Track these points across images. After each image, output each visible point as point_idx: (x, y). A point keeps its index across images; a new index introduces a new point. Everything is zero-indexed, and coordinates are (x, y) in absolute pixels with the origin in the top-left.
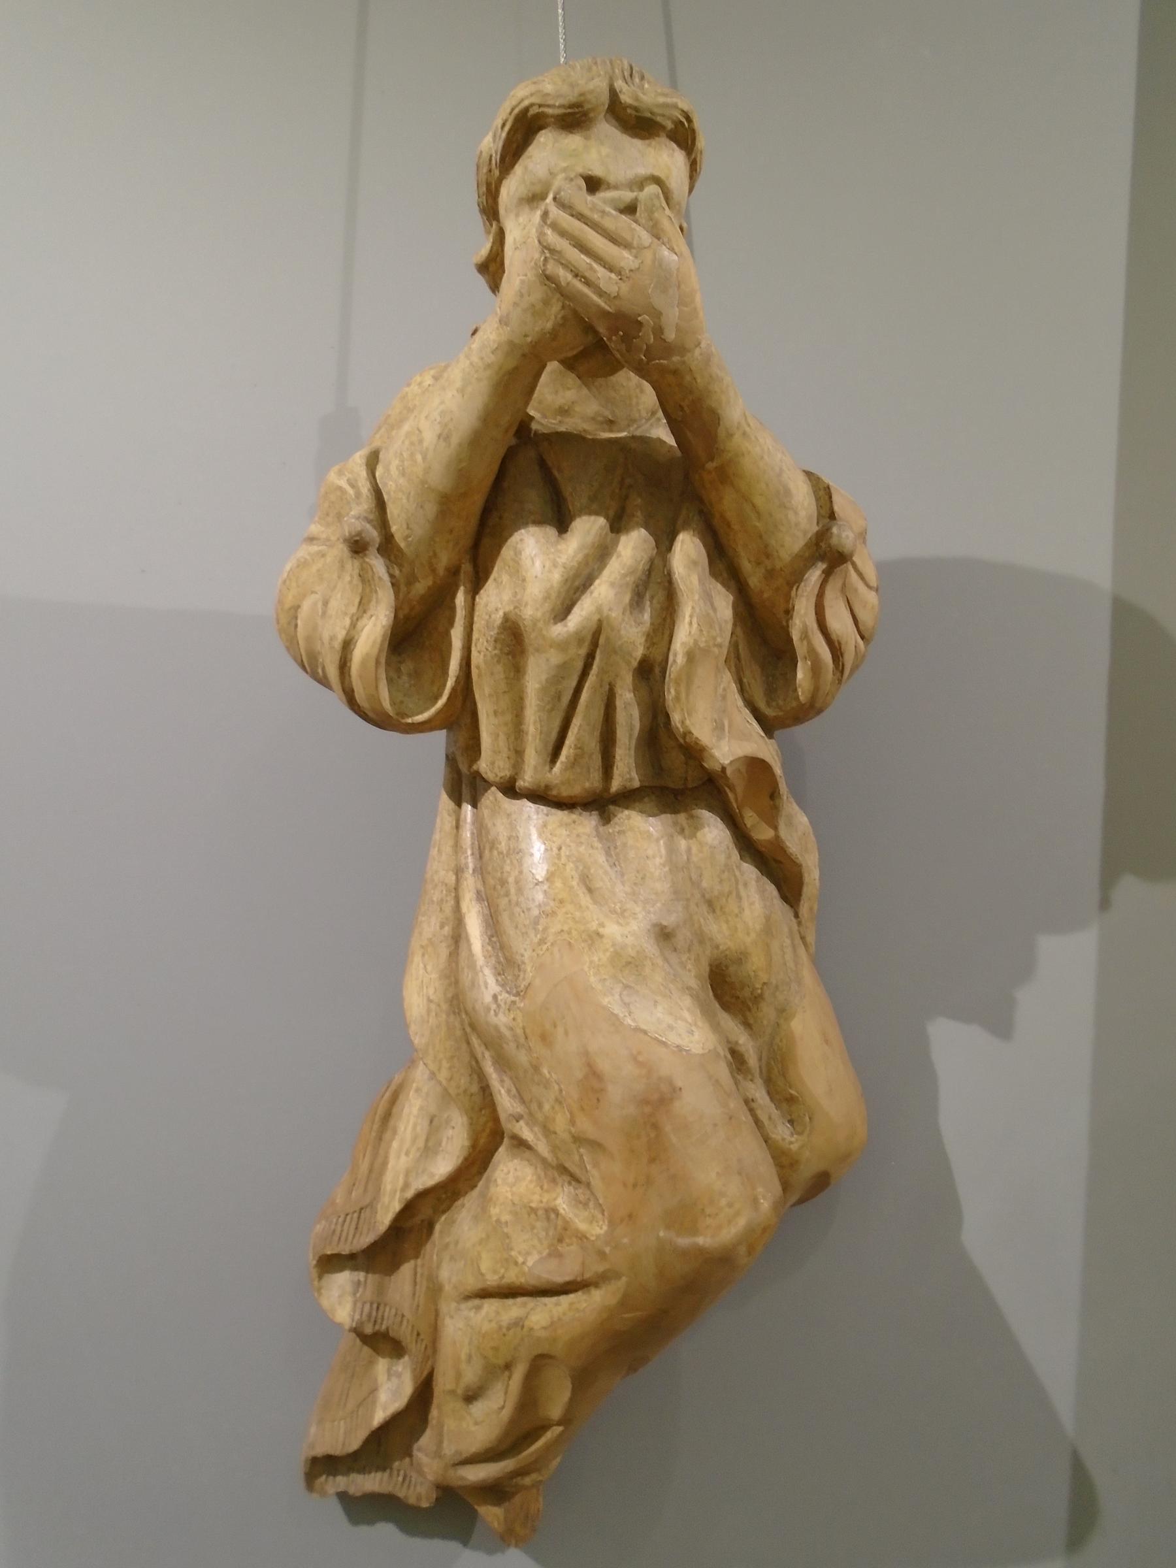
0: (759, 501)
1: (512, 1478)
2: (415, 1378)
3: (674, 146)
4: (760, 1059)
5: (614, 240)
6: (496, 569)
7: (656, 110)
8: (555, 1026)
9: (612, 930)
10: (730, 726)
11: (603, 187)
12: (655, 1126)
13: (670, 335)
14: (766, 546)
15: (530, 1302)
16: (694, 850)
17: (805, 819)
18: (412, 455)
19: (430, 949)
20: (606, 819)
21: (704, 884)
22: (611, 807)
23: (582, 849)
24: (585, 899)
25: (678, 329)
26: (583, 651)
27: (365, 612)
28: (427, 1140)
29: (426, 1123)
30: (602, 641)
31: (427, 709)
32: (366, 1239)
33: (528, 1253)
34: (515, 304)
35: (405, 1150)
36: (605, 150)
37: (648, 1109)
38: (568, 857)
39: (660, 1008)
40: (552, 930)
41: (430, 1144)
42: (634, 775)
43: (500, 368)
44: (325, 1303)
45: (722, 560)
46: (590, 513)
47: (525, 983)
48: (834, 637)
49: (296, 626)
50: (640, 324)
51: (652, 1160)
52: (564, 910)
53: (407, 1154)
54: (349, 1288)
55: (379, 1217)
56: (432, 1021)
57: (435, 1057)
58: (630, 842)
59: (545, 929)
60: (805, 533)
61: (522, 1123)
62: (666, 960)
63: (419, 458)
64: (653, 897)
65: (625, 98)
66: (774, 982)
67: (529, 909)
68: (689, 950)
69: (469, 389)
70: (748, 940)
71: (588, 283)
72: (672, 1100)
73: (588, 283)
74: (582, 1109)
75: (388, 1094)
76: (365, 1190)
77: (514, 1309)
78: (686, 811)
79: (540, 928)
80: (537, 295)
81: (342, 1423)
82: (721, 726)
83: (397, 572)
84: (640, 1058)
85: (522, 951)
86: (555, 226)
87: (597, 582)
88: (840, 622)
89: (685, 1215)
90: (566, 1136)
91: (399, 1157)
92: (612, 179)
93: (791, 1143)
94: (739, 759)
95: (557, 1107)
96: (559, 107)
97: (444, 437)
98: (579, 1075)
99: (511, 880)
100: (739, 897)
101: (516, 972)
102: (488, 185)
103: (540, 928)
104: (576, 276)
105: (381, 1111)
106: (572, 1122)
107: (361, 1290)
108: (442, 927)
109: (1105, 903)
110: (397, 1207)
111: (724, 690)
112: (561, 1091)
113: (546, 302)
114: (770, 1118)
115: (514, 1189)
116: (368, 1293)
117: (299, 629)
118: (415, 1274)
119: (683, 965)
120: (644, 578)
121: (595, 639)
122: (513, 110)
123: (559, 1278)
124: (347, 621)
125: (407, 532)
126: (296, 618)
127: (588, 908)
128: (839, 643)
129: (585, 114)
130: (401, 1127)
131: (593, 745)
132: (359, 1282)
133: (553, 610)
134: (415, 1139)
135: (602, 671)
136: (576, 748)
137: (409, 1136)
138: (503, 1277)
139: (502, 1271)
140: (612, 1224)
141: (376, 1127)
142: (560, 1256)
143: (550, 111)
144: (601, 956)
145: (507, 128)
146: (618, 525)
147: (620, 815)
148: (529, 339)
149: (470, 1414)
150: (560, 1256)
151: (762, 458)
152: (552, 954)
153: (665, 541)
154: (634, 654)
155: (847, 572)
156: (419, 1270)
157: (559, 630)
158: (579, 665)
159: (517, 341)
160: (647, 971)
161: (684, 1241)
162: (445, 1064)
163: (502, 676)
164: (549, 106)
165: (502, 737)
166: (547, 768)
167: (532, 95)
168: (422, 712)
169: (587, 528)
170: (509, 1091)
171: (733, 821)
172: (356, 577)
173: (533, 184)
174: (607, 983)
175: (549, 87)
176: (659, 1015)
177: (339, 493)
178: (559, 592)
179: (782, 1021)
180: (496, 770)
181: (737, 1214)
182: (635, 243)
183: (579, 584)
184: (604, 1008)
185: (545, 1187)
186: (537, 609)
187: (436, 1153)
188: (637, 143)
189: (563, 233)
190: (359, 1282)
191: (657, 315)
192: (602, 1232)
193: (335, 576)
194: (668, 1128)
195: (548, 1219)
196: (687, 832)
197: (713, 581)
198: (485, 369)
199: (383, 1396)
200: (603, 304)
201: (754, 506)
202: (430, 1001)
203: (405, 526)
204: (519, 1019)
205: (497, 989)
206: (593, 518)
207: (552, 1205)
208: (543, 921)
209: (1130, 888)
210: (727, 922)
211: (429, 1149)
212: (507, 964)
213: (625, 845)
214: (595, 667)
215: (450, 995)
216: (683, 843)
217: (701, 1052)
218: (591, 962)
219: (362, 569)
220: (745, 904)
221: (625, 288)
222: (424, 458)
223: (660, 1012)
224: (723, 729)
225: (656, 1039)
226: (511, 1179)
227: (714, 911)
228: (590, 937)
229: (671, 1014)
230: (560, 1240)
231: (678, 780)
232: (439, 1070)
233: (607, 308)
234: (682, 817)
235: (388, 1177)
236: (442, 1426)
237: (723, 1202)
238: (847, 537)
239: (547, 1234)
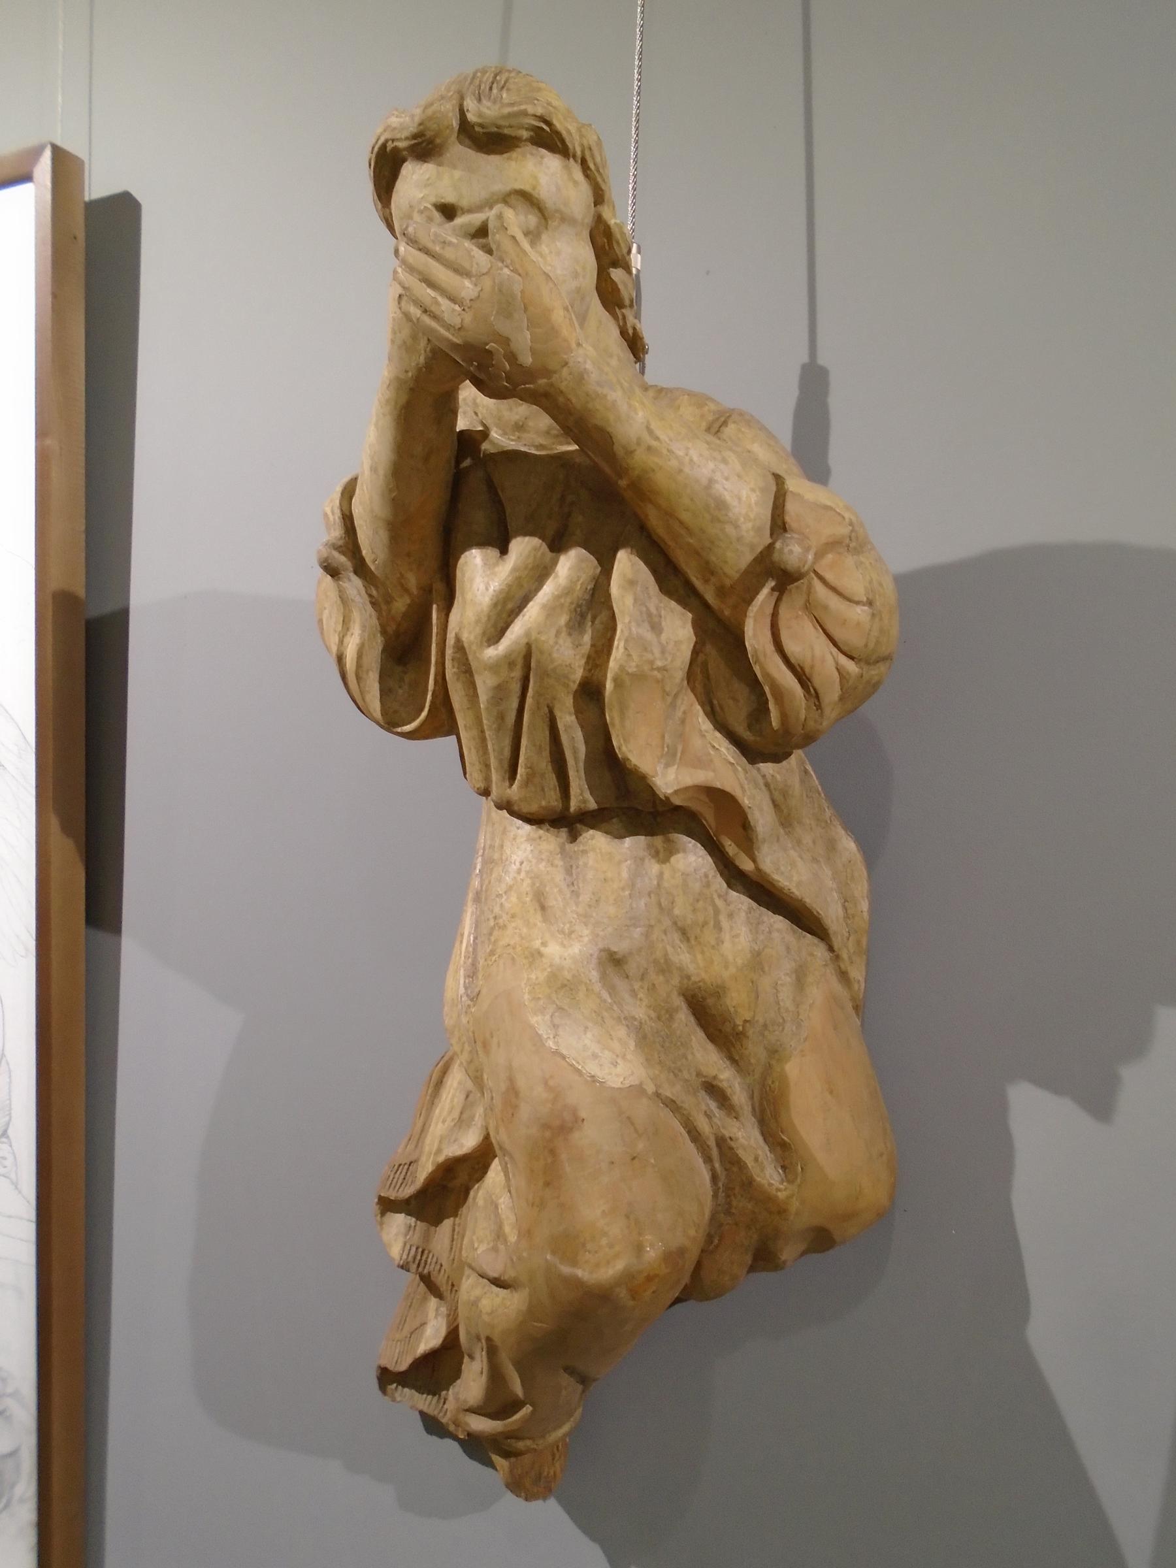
0: (685, 516)
1: (508, 1438)
2: (448, 1327)
3: (543, 151)
4: (752, 1098)
7: (502, 123)
9: (553, 950)
10: (683, 752)
11: (459, 213)
12: (553, 1152)
13: (527, 360)
14: (707, 563)
16: (667, 875)
17: (852, 846)
20: (574, 837)
21: (676, 911)
22: (578, 826)
23: (542, 866)
24: (537, 918)
25: (533, 351)
26: (517, 673)
29: (463, 1097)
30: (533, 665)
31: (414, 720)
32: (408, 1191)
33: (481, 1242)
36: (457, 174)
37: (548, 1134)
38: (527, 872)
39: (589, 1035)
40: (502, 943)
41: (465, 1116)
42: (588, 795)
43: (396, 403)
45: (671, 576)
46: (525, 535)
47: (477, 990)
48: (793, 661)
50: (490, 352)
51: (547, 1184)
52: (513, 925)
53: (444, 1122)
54: (403, 1230)
57: (459, 1039)
58: (591, 863)
60: (752, 547)
62: (612, 990)
64: (605, 920)
65: (471, 117)
66: (761, 1021)
68: (642, 979)
70: (726, 974)
71: (434, 317)
72: (571, 1130)
73: (434, 317)
78: (663, 834)
82: (678, 752)
83: (374, 593)
84: (551, 1083)
87: (531, 604)
88: (805, 641)
89: (568, 1244)
92: (464, 203)
93: (778, 1190)
94: (687, 789)
96: (407, 138)
100: (718, 927)
103: (493, 939)
104: (425, 311)
111: (684, 713)
114: (756, 1159)
116: (416, 1238)
118: (454, 1230)
119: (634, 994)
120: (587, 597)
121: (526, 661)
125: (373, 556)
127: (535, 925)
128: (802, 668)
129: (431, 142)
131: (544, 765)
133: (484, 633)
135: (538, 694)
136: (527, 767)
137: (447, 1107)
144: (538, 975)
146: (557, 545)
147: (584, 835)
148: (410, 374)
151: (681, 471)
154: (572, 677)
155: (810, 587)
157: (492, 653)
158: (516, 687)
159: (402, 377)
160: (581, 995)
161: (566, 1270)
166: (507, 783)
168: (410, 723)
169: (522, 547)
171: (714, 848)
174: (541, 1002)
176: (588, 1042)
178: (489, 617)
179: (773, 1062)
181: (617, 1256)
182: (474, 272)
183: (509, 608)
184: (532, 1027)
187: (469, 1126)
188: (494, 159)
191: (506, 341)
194: (564, 1156)
196: (661, 855)
197: (666, 599)
199: (429, 1331)
200: (451, 337)
201: (681, 523)
206: (527, 539)
208: (496, 933)
210: (703, 952)
213: (586, 865)
214: (530, 690)
216: (654, 868)
217: (619, 1085)
218: (528, 979)
220: (727, 937)
221: (468, 318)
223: (588, 1040)
224: (675, 755)
225: (572, 1065)
227: (688, 940)
228: (532, 955)
229: (599, 1042)
231: (631, 806)
233: (455, 340)
234: (658, 840)
235: (428, 1141)
237: (604, 1241)
238: (791, 552)
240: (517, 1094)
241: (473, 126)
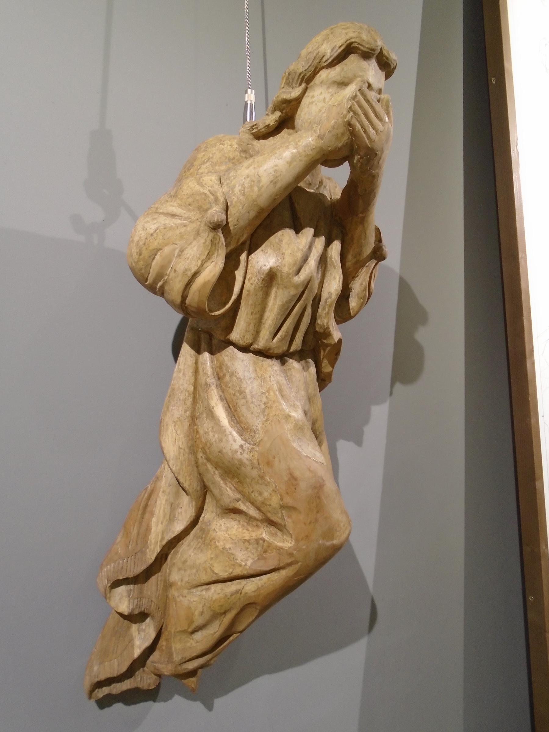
5: (377, 115)
6: (264, 245)
8: (274, 458)
9: (293, 414)
15: (244, 582)
18: (251, 186)
19: (178, 423)
20: (283, 363)
22: (286, 358)
27: (209, 259)
28: (170, 515)
33: (247, 560)
34: (330, 131)
35: (160, 522)
39: (310, 447)
44: (113, 604)
49: (154, 258)
51: (318, 512)
53: (162, 523)
54: (125, 594)
55: (148, 556)
56: (181, 458)
59: (268, 414)
61: (240, 502)
63: (256, 189)
67: (259, 405)
69: (294, 163)
71: (365, 131)
72: (323, 485)
73: (365, 131)
74: (287, 493)
75: (146, 495)
76: (137, 544)
77: (233, 586)
79: (266, 413)
80: (340, 130)
81: (115, 660)
85: (257, 425)
86: (358, 103)
87: (309, 259)
90: (277, 506)
91: (157, 526)
95: (273, 494)
96: (367, 48)
97: (273, 182)
98: (286, 479)
99: (247, 391)
101: (252, 434)
102: (316, 68)
103: (266, 413)
105: (143, 504)
106: (282, 499)
107: (132, 593)
108: (186, 412)
109: (391, 393)
110: (158, 549)
112: (276, 486)
113: (343, 134)
115: (229, 533)
117: (155, 261)
122: (347, 40)
123: (267, 569)
124: (199, 263)
125: (236, 223)
126: (156, 255)
130: (157, 511)
132: (131, 590)
134: (165, 515)
138: (232, 573)
139: (231, 570)
140: (297, 540)
141: (140, 512)
142: (265, 559)
143: (362, 48)
145: (342, 48)
148: (330, 149)
149: (193, 639)
150: (265, 559)
152: (271, 425)
153: (328, 243)
156: (159, 578)
161: (329, 543)
162: (188, 478)
163: (261, 297)
164: (362, 45)
165: (252, 325)
167: (357, 37)
169: (309, 232)
170: (231, 488)
172: (208, 242)
173: (344, 77)
175: (365, 37)
177: (203, 196)
180: (245, 339)
185: (250, 529)
186: (290, 269)
187: (173, 521)
189: (361, 107)
190: (131, 590)
192: (292, 545)
193: (192, 238)
194: (323, 498)
195: (258, 544)
198: (305, 156)
199: (137, 642)
202: (180, 448)
203: (236, 220)
204: (256, 456)
205: (243, 442)
207: (261, 537)
209: (398, 386)
211: (171, 519)
212: (244, 429)
213: (291, 375)
215: (189, 445)
219: (214, 237)
222: (259, 190)
226: (223, 528)
228: (286, 417)
230: (265, 552)
232: (185, 481)
234: (303, 362)
236: (171, 648)
239: (257, 550)
240: (296, 479)
241: (383, 56)
